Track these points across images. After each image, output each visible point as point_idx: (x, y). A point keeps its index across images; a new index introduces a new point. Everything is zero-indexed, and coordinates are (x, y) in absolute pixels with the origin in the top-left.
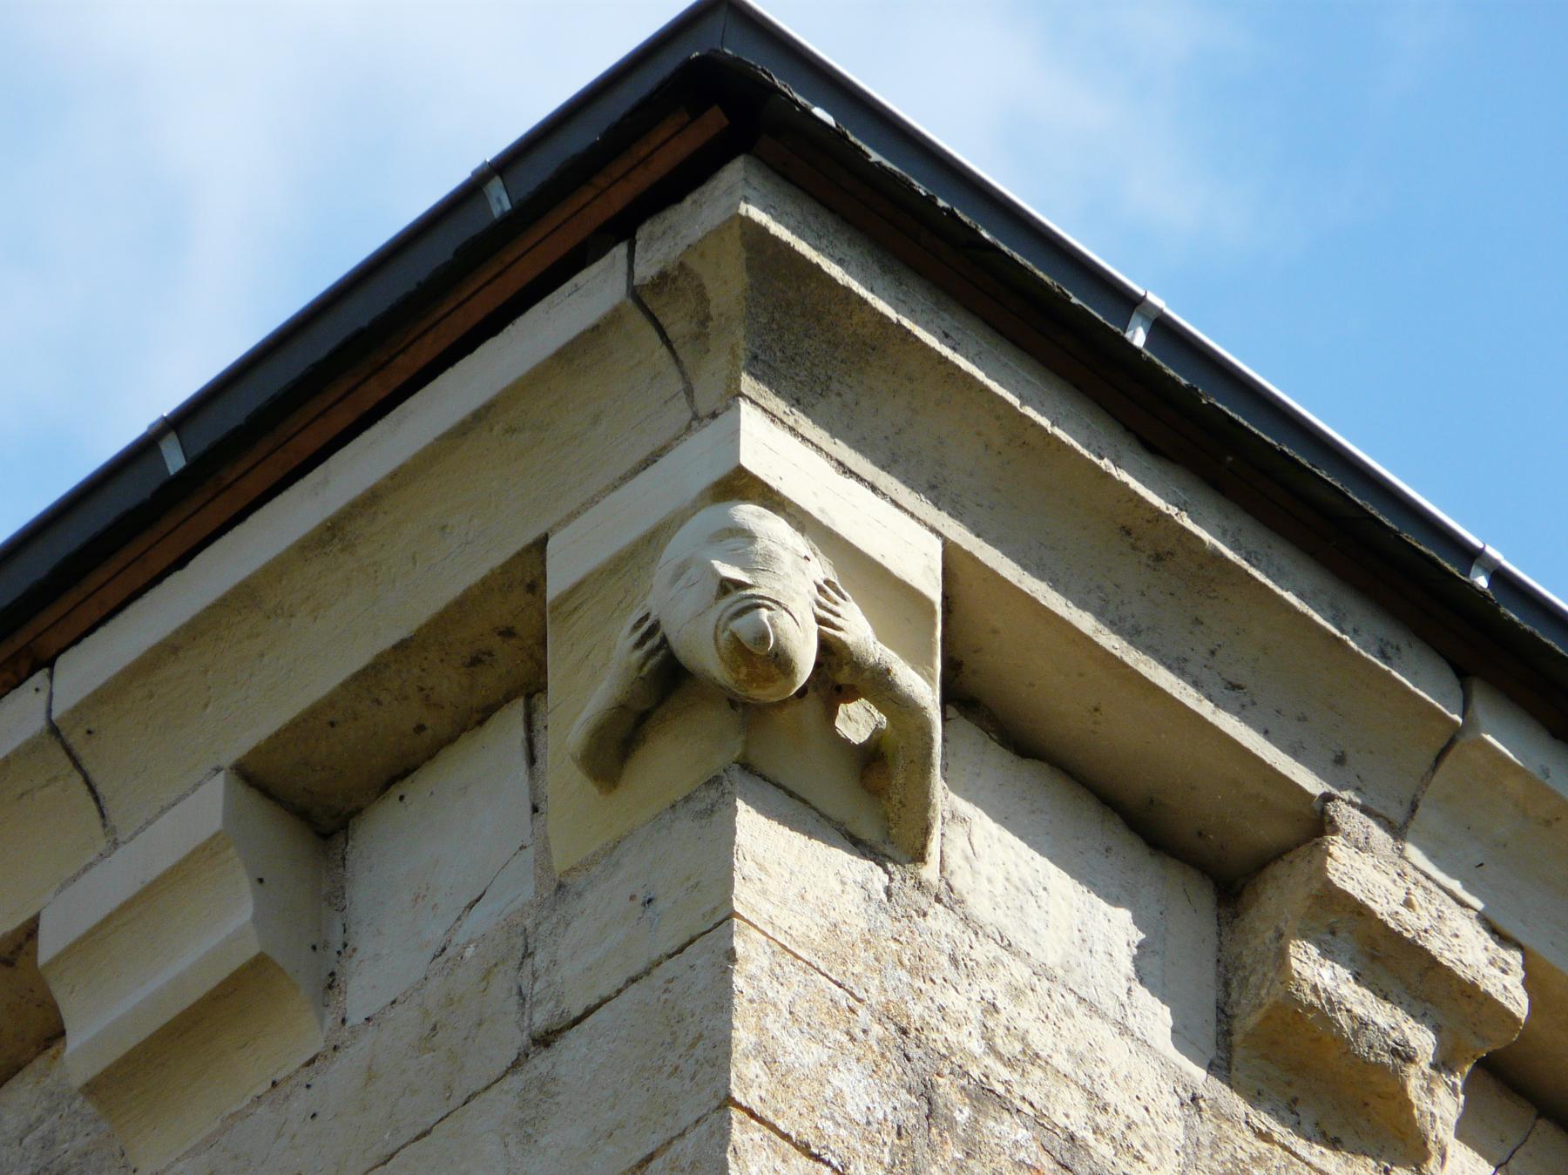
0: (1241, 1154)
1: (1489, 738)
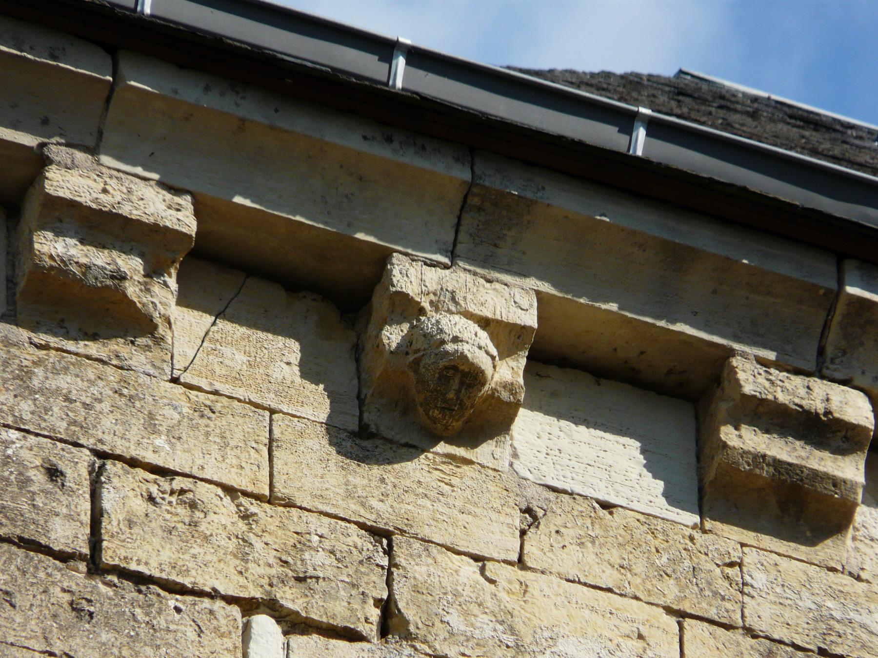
0: (25, 363)
1: (133, 83)
